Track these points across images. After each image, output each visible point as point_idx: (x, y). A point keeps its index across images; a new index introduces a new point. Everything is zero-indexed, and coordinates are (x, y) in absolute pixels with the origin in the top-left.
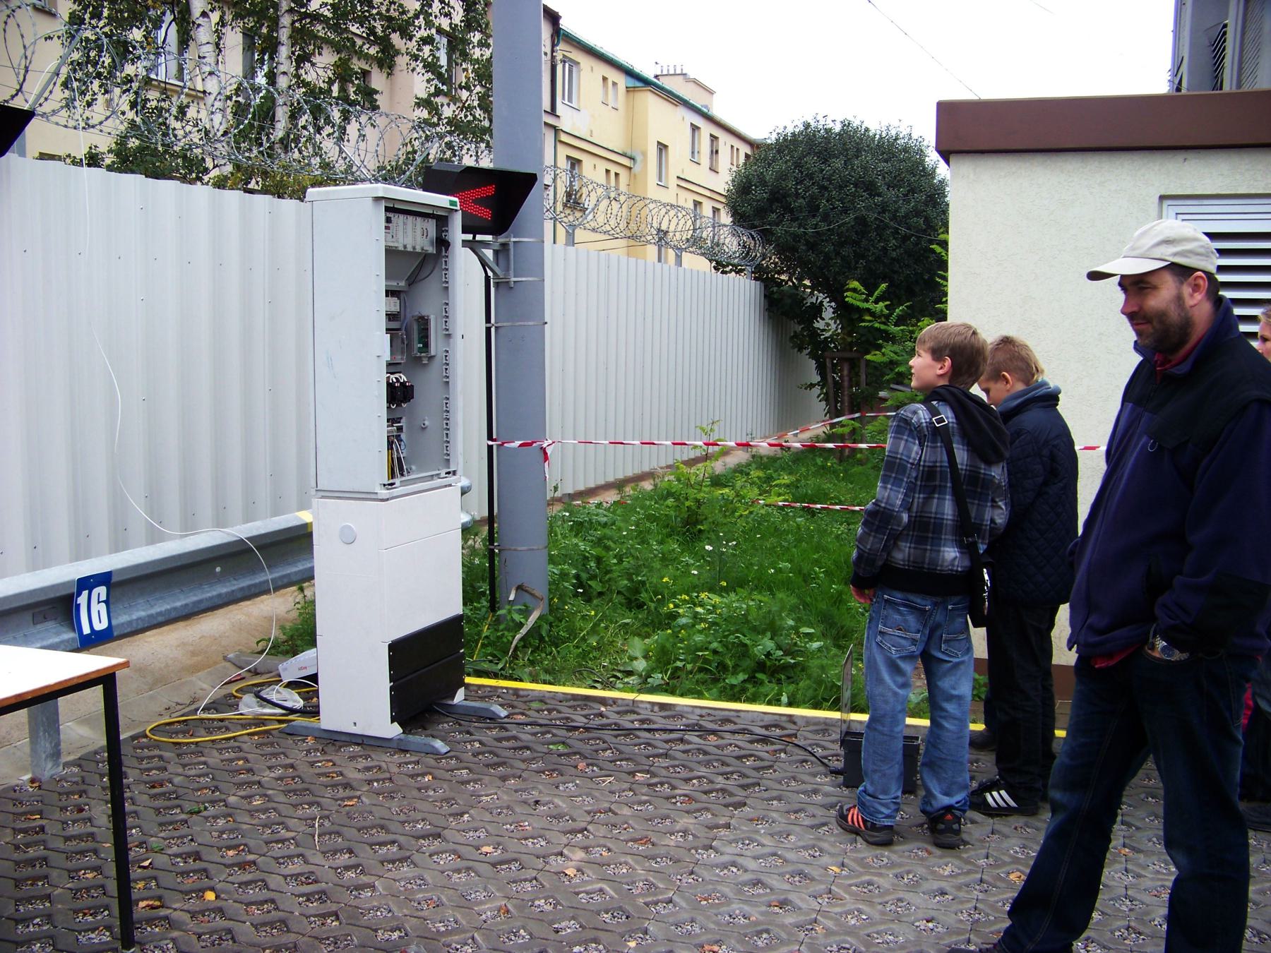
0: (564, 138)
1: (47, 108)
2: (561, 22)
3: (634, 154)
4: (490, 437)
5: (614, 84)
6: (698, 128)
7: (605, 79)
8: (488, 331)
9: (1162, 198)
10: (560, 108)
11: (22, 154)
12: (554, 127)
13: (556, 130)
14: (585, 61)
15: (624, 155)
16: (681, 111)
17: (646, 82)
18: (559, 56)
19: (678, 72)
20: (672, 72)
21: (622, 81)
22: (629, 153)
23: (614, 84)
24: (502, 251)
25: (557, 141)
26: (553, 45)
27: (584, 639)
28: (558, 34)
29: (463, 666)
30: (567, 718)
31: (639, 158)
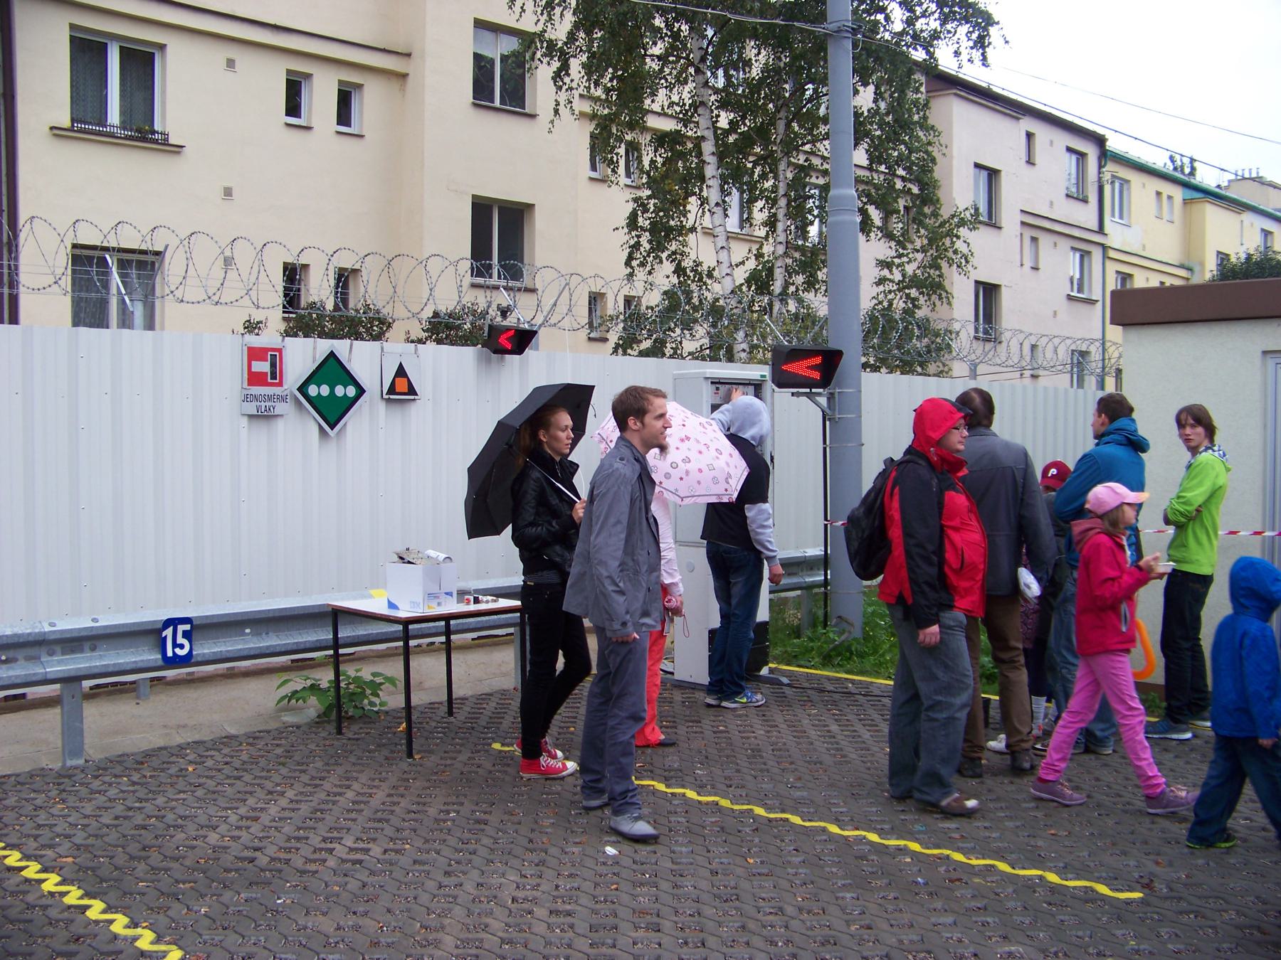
0: (1112, 254)
1: (618, 283)
2: (1108, 143)
3: (1191, 265)
4: (826, 519)
5: (1170, 197)
6: (1271, 233)
7: (1159, 194)
8: (825, 449)
9: (1265, 353)
10: (1107, 229)
11: (537, 349)
12: (1102, 245)
13: (1104, 248)
14: (1135, 178)
15: (1182, 266)
16: (1248, 217)
17: (1206, 192)
18: (1107, 177)
19: (1254, 175)
20: (1247, 175)
21: (1178, 193)
22: (1187, 264)
23: (1170, 197)
24: (831, 398)
25: (1105, 257)
26: (1100, 167)
27: (883, 655)
28: (1105, 155)
29: (766, 654)
30: (1128, 803)
31: (1196, 269)
